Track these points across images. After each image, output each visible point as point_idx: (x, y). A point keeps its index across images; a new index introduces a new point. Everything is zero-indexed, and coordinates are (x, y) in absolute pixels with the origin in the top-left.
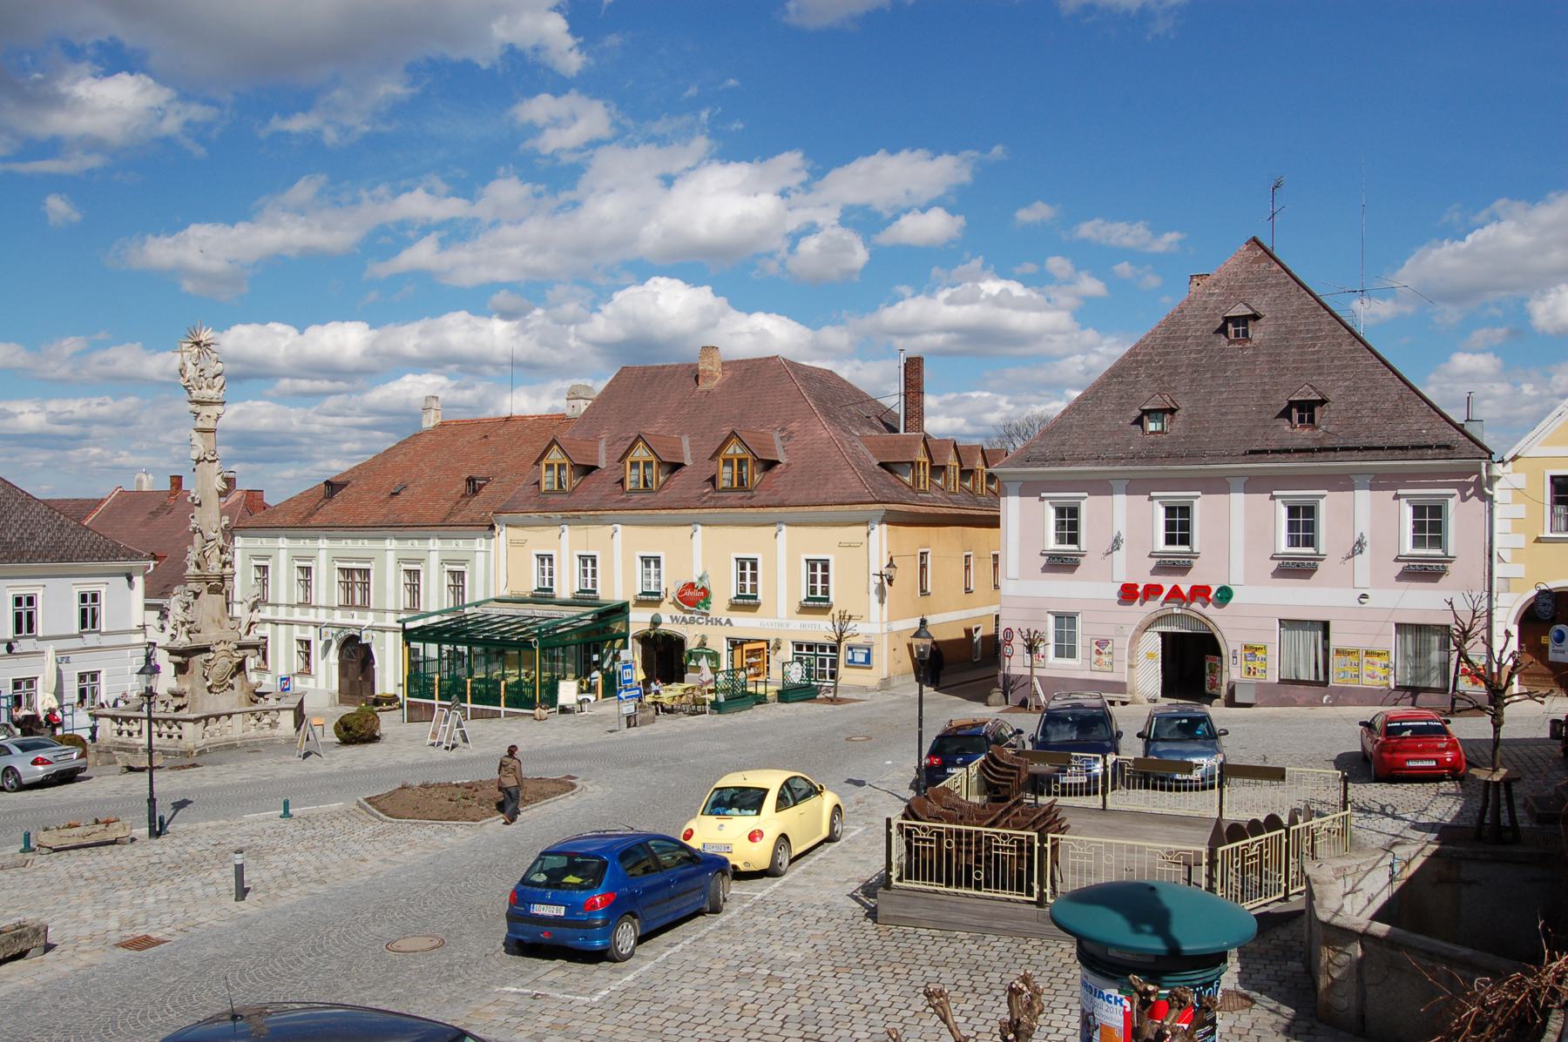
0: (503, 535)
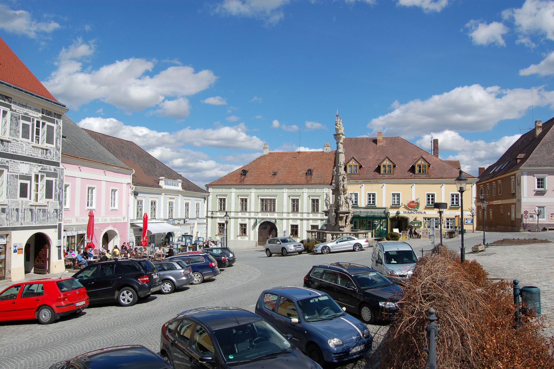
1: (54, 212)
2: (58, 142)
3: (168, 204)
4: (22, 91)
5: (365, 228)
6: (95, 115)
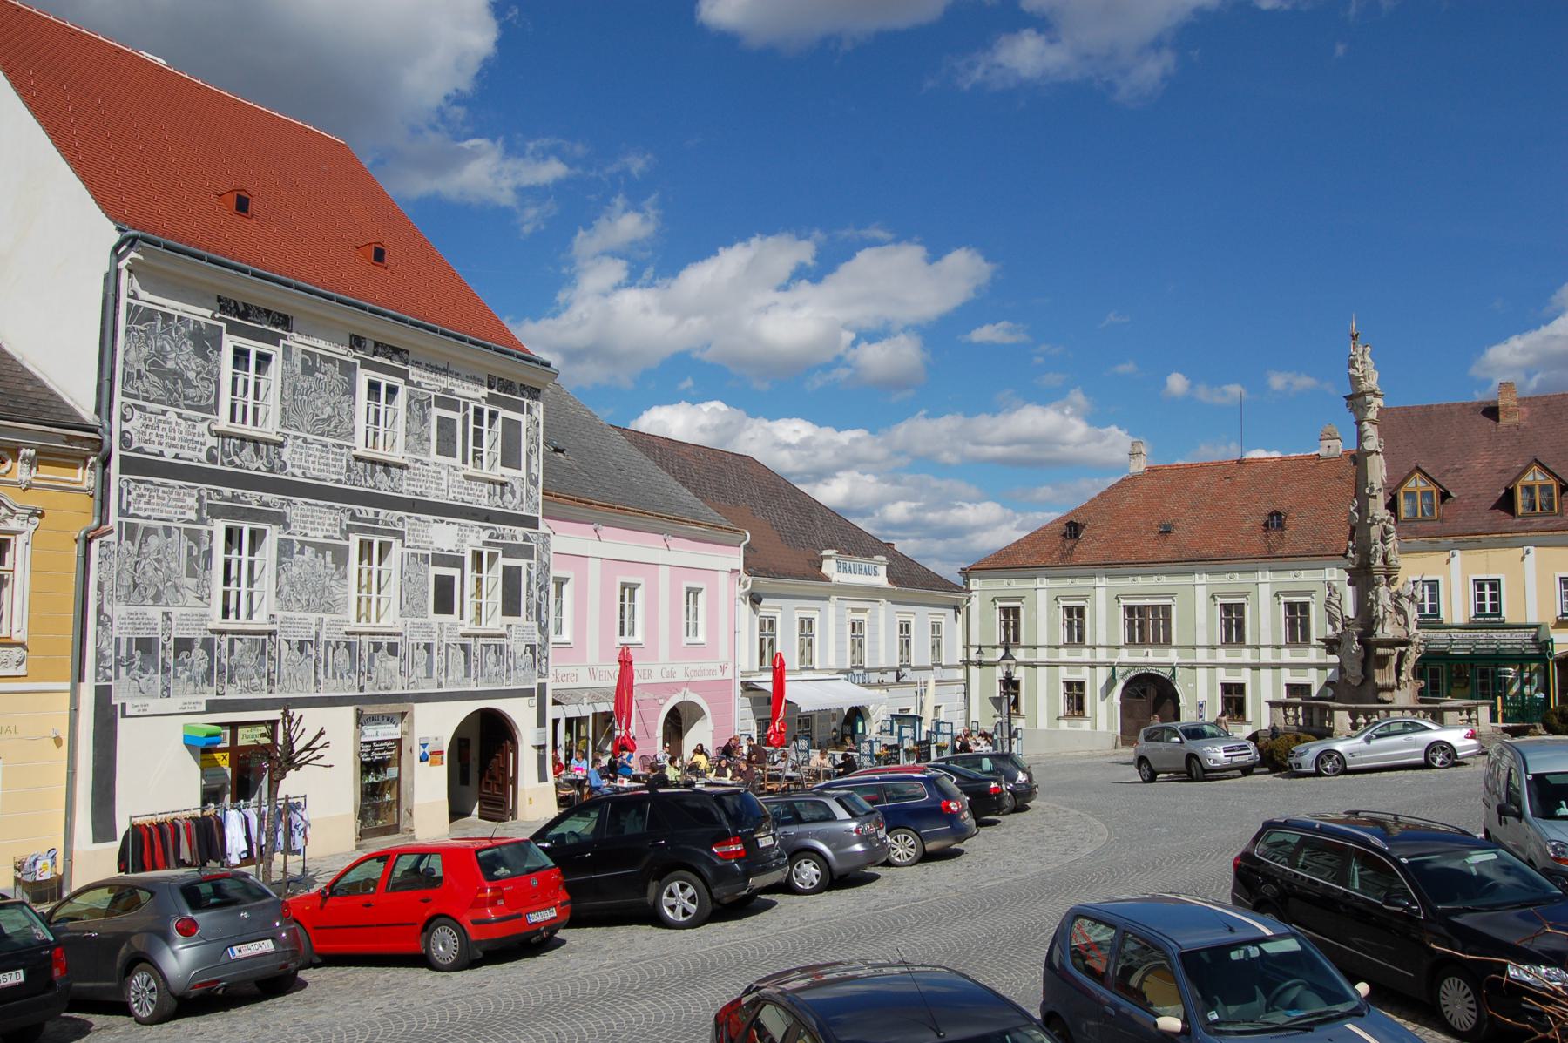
1: (525, 653)
3: (849, 628)
4: (435, 331)
5: (1468, 689)
6: (669, 398)
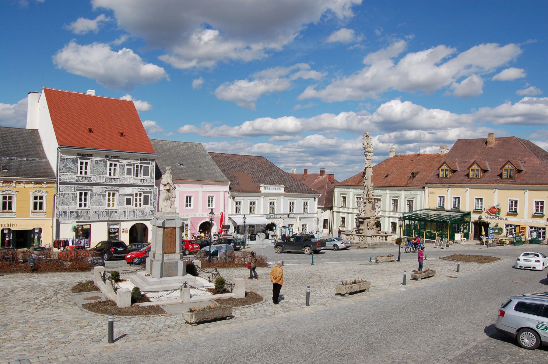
0: (427, 190)
2: (153, 174)
